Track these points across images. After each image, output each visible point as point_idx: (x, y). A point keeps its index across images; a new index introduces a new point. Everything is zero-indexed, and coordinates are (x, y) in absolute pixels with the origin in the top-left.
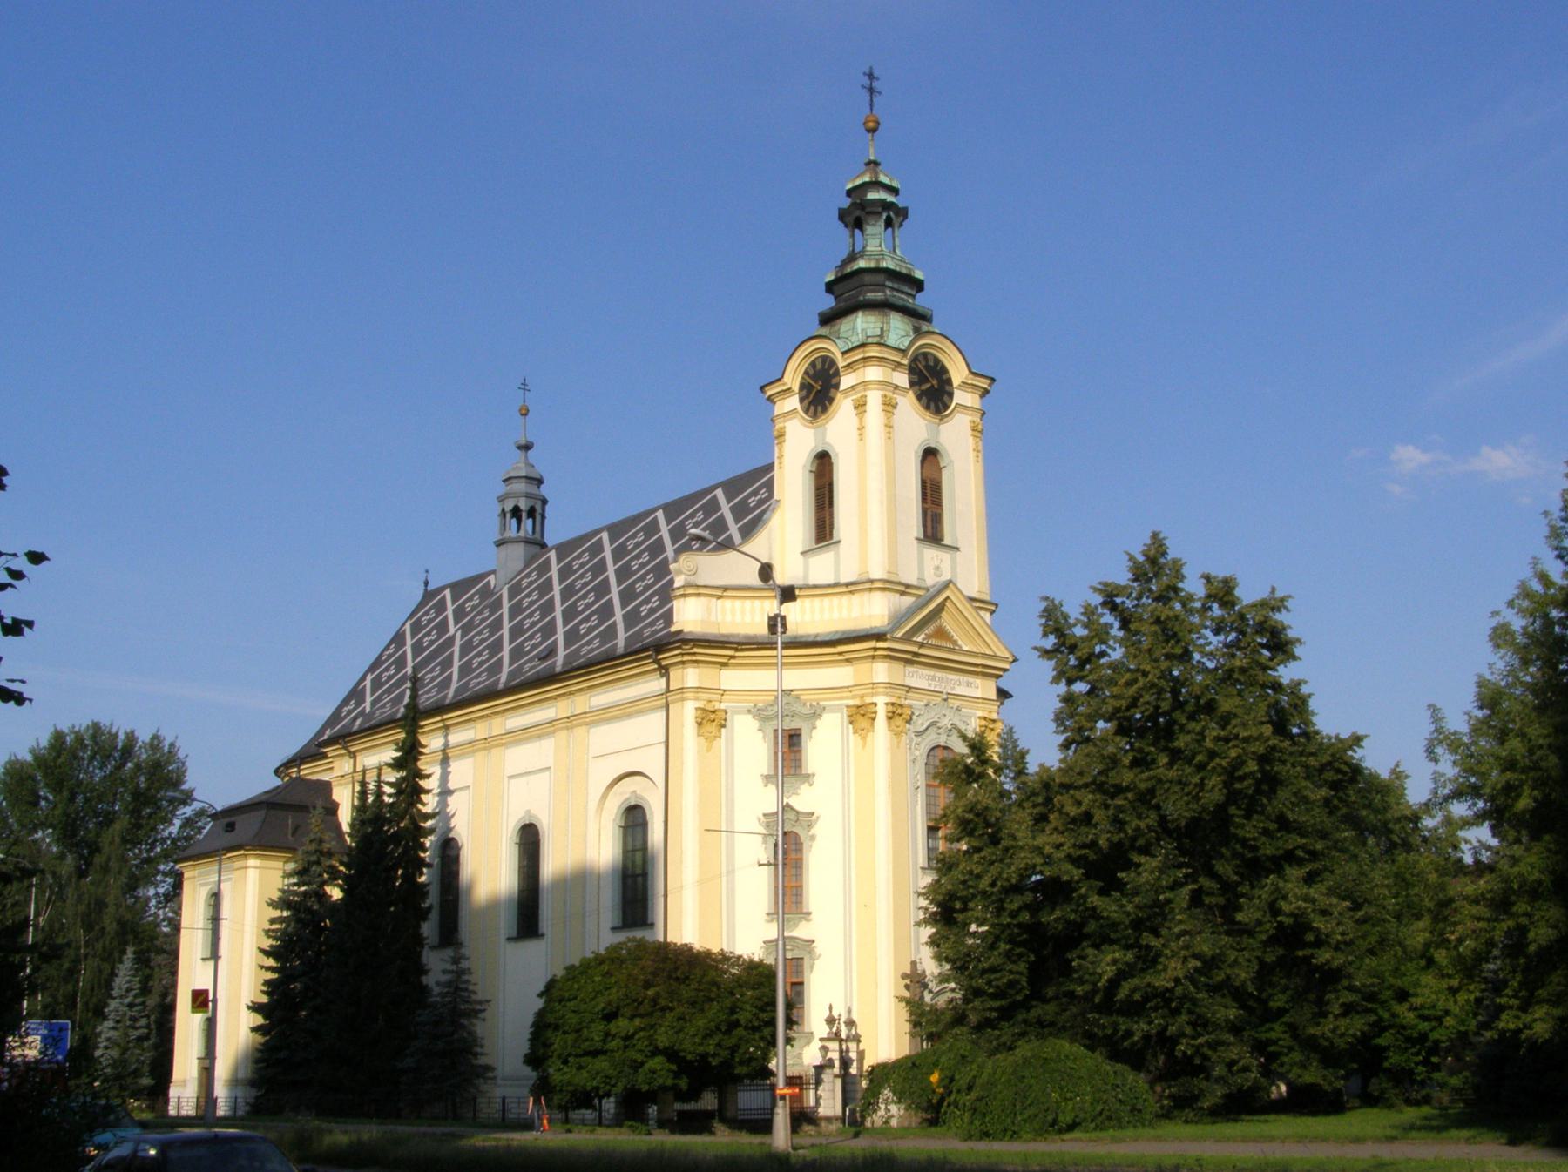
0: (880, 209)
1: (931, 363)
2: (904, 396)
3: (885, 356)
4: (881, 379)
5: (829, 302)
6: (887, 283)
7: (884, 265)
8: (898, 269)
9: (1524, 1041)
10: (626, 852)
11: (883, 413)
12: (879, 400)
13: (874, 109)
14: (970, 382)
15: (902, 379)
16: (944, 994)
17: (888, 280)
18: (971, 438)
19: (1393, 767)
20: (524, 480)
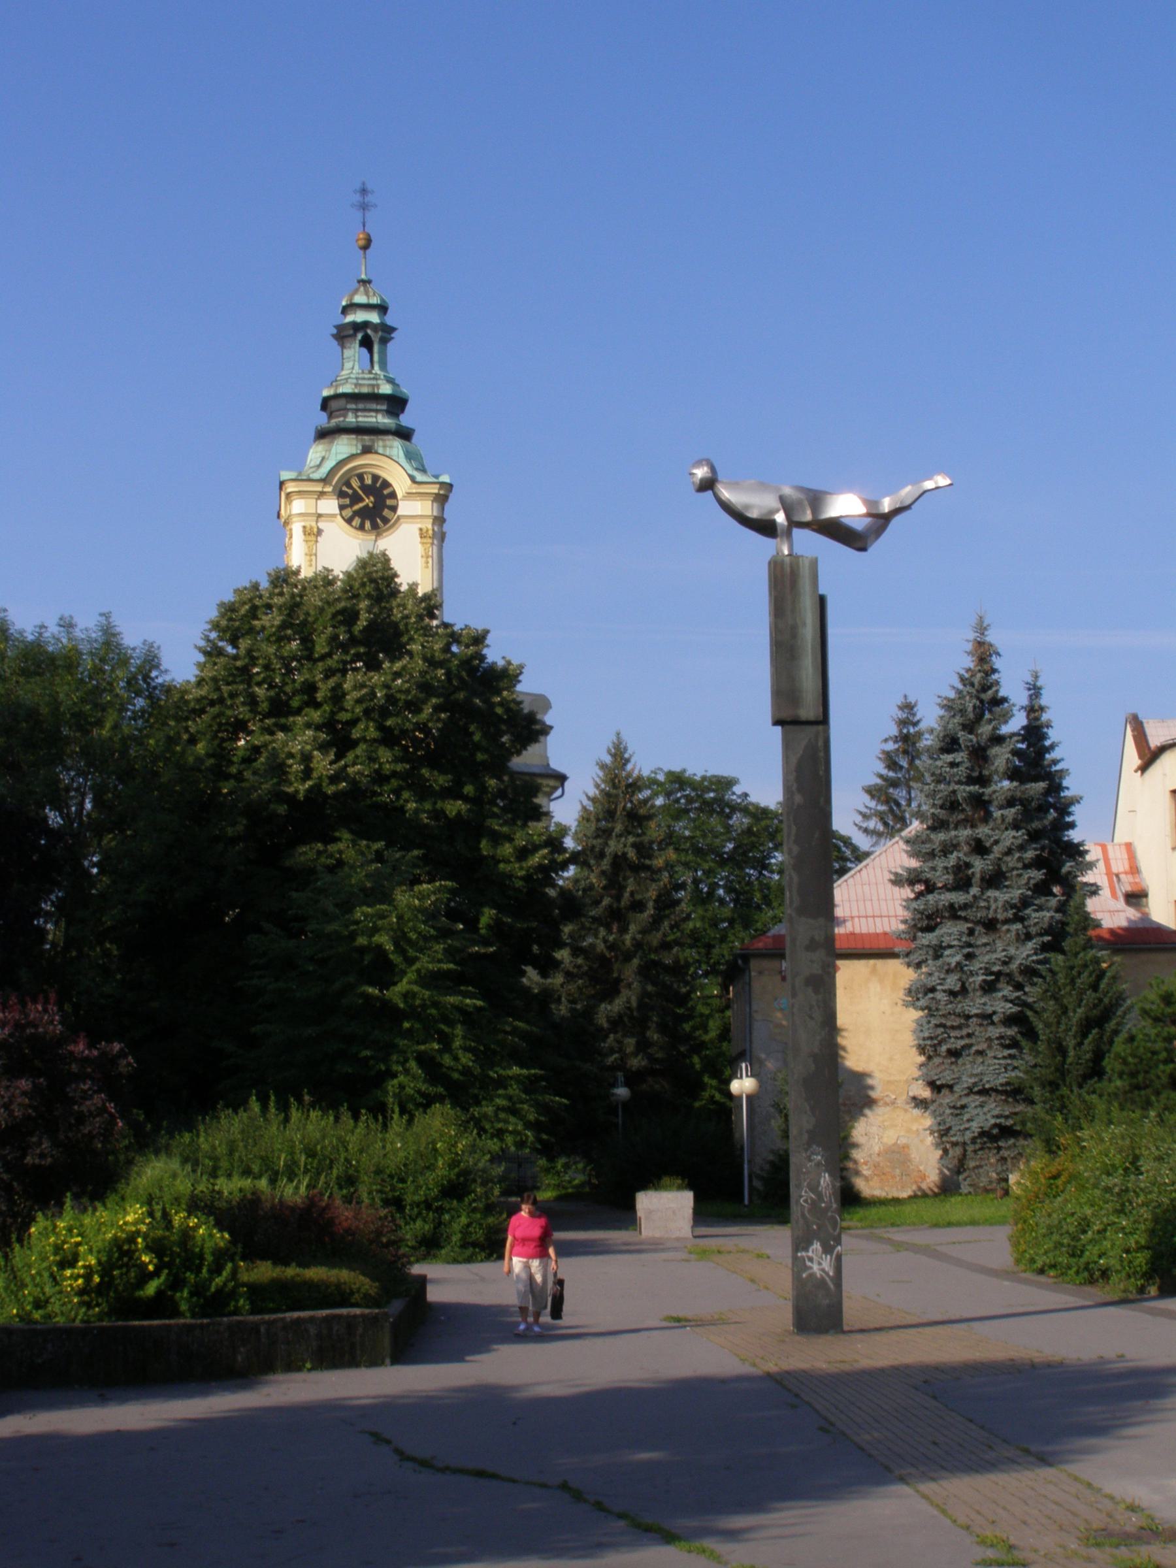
0: (351, 332)
1: (368, 481)
2: (333, 521)
3: (301, 489)
4: (303, 511)
5: (322, 420)
6: (350, 406)
7: (341, 390)
8: (356, 391)
9: (639, 861)
10: (865, 1199)
11: (304, 543)
12: (301, 529)
13: (367, 225)
14: (414, 491)
15: (330, 505)
16: (840, 1060)
17: (347, 402)
18: (420, 545)
19: (972, 635)
20: (908, 502)
